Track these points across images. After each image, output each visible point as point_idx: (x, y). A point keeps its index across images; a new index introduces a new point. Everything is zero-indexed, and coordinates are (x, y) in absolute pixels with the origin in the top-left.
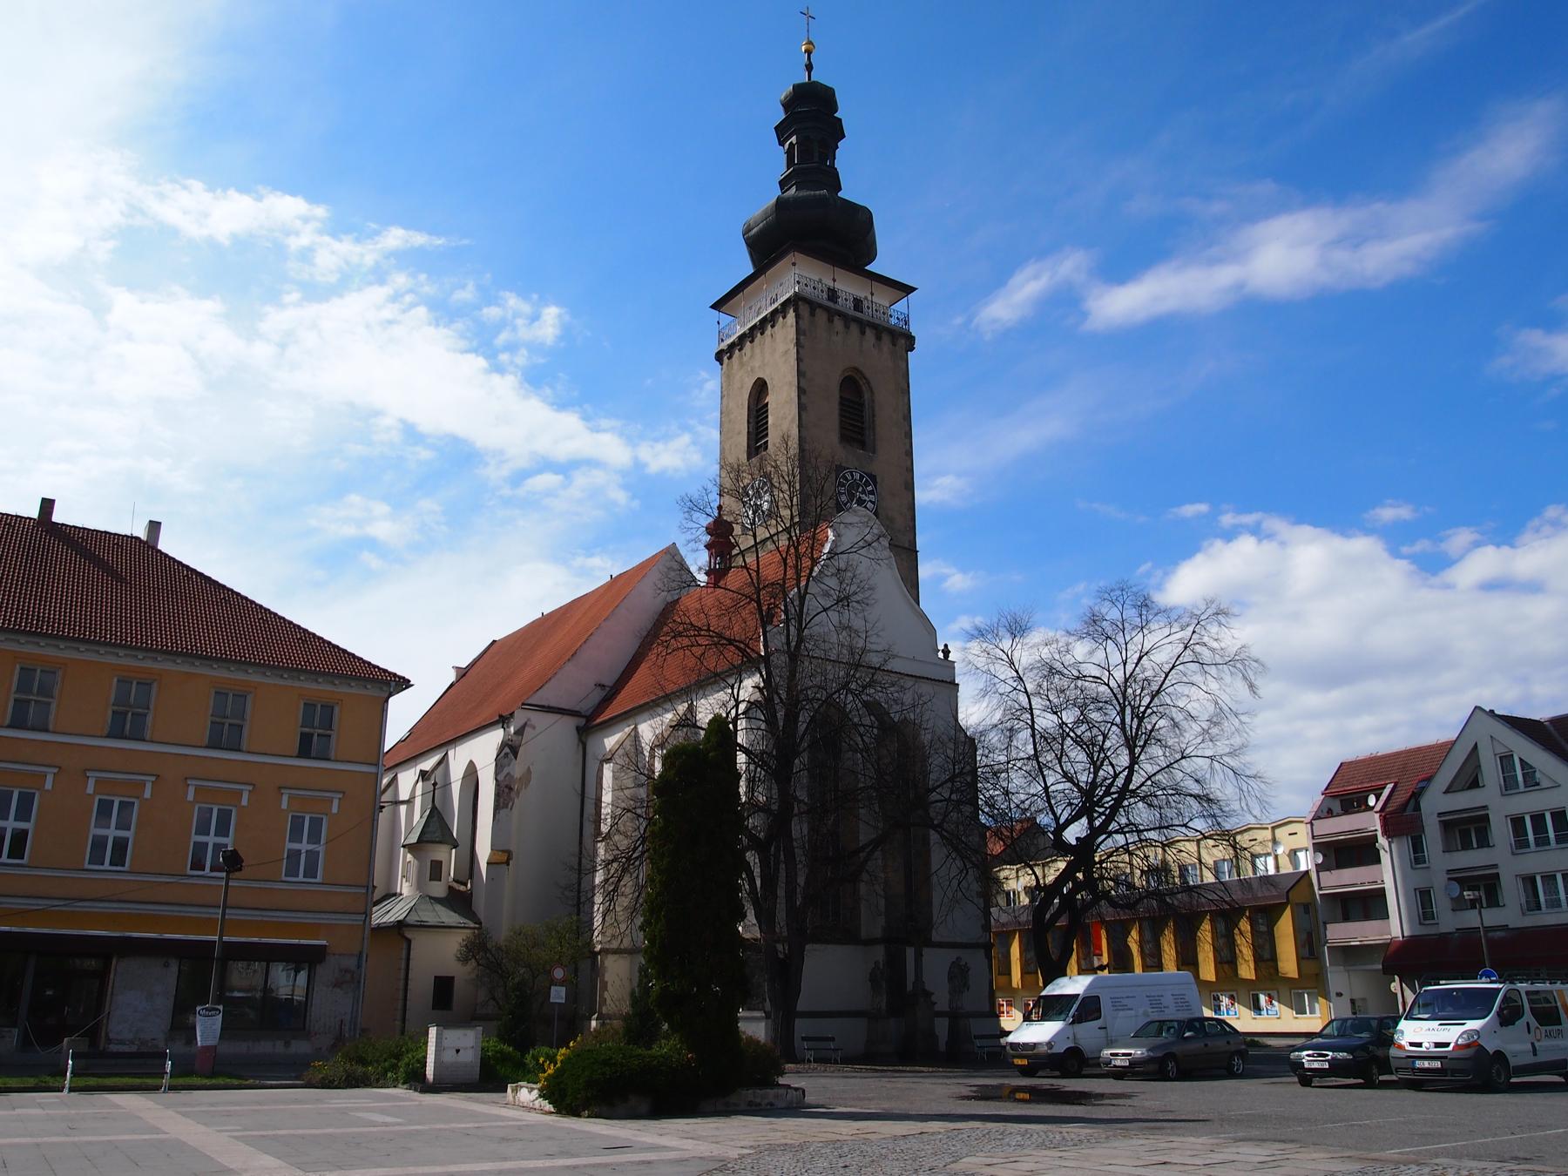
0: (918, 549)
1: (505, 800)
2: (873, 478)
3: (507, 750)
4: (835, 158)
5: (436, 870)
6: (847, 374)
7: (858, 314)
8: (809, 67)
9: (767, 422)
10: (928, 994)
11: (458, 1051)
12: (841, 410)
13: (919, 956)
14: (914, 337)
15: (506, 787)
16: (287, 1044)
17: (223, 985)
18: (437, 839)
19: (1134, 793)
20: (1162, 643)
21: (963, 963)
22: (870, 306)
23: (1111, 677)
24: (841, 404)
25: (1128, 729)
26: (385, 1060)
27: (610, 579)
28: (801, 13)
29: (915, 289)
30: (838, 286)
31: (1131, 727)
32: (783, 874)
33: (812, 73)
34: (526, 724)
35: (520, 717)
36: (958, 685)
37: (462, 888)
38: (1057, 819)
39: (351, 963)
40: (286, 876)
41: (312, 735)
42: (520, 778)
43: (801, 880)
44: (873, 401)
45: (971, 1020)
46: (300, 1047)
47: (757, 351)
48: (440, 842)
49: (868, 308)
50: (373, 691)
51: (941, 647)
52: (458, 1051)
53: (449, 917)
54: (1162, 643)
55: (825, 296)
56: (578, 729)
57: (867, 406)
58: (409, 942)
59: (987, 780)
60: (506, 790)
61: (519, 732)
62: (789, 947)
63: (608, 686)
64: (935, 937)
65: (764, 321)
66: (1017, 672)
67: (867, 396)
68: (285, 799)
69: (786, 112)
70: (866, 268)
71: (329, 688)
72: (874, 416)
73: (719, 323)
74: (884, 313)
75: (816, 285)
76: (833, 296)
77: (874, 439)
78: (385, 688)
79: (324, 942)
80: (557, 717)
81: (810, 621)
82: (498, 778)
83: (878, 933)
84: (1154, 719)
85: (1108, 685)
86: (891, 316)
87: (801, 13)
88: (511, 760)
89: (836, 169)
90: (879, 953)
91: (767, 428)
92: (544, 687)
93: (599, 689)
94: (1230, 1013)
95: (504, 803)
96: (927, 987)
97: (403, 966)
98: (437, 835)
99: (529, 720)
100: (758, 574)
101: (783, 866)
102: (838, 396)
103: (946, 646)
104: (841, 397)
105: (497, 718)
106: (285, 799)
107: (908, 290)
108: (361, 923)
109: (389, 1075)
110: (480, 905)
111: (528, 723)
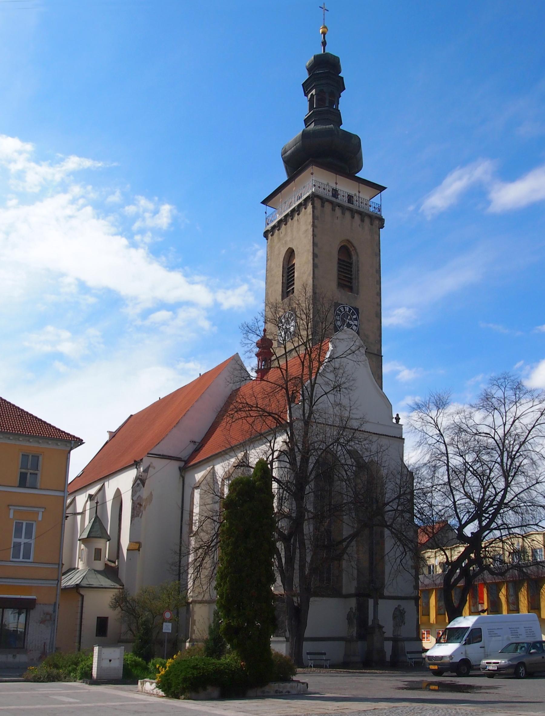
0: (382, 355)
1: (137, 512)
2: (357, 310)
3: (139, 482)
4: (338, 104)
5: (98, 554)
6: (342, 244)
7: (350, 205)
8: (324, 44)
10: (381, 627)
11: (110, 661)
12: (339, 267)
13: (376, 604)
14: (384, 219)
16: (14, 656)
18: (98, 536)
21: (401, 608)
23: (496, 433)
24: (339, 263)
25: (505, 465)
26: (70, 666)
29: (386, 188)
30: (338, 187)
33: (326, 47)
35: (147, 461)
37: (113, 565)
38: (460, 521)
39: (50, 609)
40: (13, 558)
41: (27, 473)
42: (146, 499)
44: (358, 261)
45: (405, 642)
46: (22, 658)
48: (100, 538)
50: (61, 447)
51: (394, 416)
52: (110, 661)
53: (105, 582)
55: (331, 194)
56: (180, 468)
57: (354, 265)
58: (83, 596)
60: (138, 506)
61: (146, 471)
64: (386, 593)
65: (293, 211)
66: (439, 430)
67: (354, 258)
68: (12, 512)
71: (36, 445)
72: (358, 271)
73: (266, 213)
74: (366, 204)
78: (68, 445)
79: (34, 597)
86: (370, 206)
88: (141, 488)
89: (339, 111)
90: (353, 602)
92: (161, 444)
93: (192, 444)
95: (137, 514)
96: (380, 623)
97: (79, 611)
98: (98, 533)
99: (151, 463)
102: (337, 258)
103: (398, 415)
104: (339, 259)
105: (133, 462)
106: (12, 512)
107: (381, 189)
108: (56, 586)
109: (72, 674)
110: (123, 575)
111: (151, 465)
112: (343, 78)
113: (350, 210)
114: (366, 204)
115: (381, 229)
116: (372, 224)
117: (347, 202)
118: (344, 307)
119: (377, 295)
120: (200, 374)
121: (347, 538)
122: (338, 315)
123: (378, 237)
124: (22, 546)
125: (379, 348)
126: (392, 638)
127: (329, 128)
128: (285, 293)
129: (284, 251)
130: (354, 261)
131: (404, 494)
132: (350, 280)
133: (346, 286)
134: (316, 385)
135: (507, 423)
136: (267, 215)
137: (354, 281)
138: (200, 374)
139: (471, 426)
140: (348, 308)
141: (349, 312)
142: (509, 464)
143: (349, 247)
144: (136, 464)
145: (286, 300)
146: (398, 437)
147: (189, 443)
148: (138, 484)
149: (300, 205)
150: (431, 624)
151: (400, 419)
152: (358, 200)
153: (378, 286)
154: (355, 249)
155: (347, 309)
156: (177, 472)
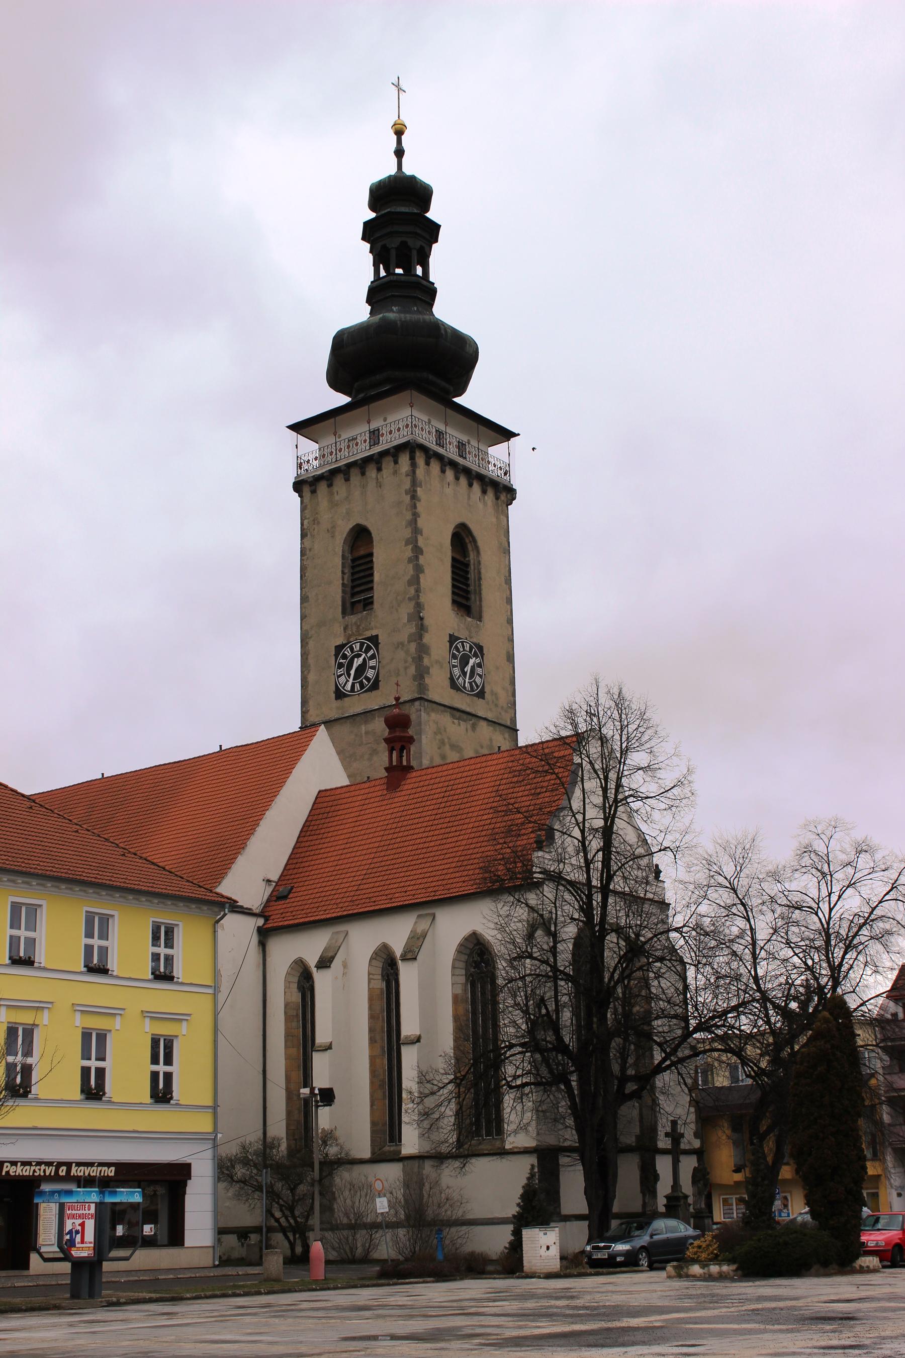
2: (480, 648)
7: (440, 450)
8: (399, 153)
12: (453, 586)
14: (515, 490)
17: (891, 1184)
20: (864, 878)
24: (453, 566)
28: (404, 91)
33: (404, 159)
44: (479, 563)
47: (357, 493)
57: (472, 567)
63: (274, 882)
67: (472, 556)
72: (480, 579)
87: (404, 91)
94: (783, 1214)
104: (453, 559)
107: (506, 435)
116: (497, 498)
117: (434, 443)
118: (462, 643)
119: (508, 623)
120: (221, 746)
122: (340, 666)
124: (20, 1032)
128: (348, 605)
129: (344, 528)
130: (472, 562)
137: (473, 597)
140: (468, 645)
141: (470, 651)
143: (464, 536)
145: (353, 619)
150: (558, 1160)
153: (509, 607)
154: (474, 540)
155: (467, 648)
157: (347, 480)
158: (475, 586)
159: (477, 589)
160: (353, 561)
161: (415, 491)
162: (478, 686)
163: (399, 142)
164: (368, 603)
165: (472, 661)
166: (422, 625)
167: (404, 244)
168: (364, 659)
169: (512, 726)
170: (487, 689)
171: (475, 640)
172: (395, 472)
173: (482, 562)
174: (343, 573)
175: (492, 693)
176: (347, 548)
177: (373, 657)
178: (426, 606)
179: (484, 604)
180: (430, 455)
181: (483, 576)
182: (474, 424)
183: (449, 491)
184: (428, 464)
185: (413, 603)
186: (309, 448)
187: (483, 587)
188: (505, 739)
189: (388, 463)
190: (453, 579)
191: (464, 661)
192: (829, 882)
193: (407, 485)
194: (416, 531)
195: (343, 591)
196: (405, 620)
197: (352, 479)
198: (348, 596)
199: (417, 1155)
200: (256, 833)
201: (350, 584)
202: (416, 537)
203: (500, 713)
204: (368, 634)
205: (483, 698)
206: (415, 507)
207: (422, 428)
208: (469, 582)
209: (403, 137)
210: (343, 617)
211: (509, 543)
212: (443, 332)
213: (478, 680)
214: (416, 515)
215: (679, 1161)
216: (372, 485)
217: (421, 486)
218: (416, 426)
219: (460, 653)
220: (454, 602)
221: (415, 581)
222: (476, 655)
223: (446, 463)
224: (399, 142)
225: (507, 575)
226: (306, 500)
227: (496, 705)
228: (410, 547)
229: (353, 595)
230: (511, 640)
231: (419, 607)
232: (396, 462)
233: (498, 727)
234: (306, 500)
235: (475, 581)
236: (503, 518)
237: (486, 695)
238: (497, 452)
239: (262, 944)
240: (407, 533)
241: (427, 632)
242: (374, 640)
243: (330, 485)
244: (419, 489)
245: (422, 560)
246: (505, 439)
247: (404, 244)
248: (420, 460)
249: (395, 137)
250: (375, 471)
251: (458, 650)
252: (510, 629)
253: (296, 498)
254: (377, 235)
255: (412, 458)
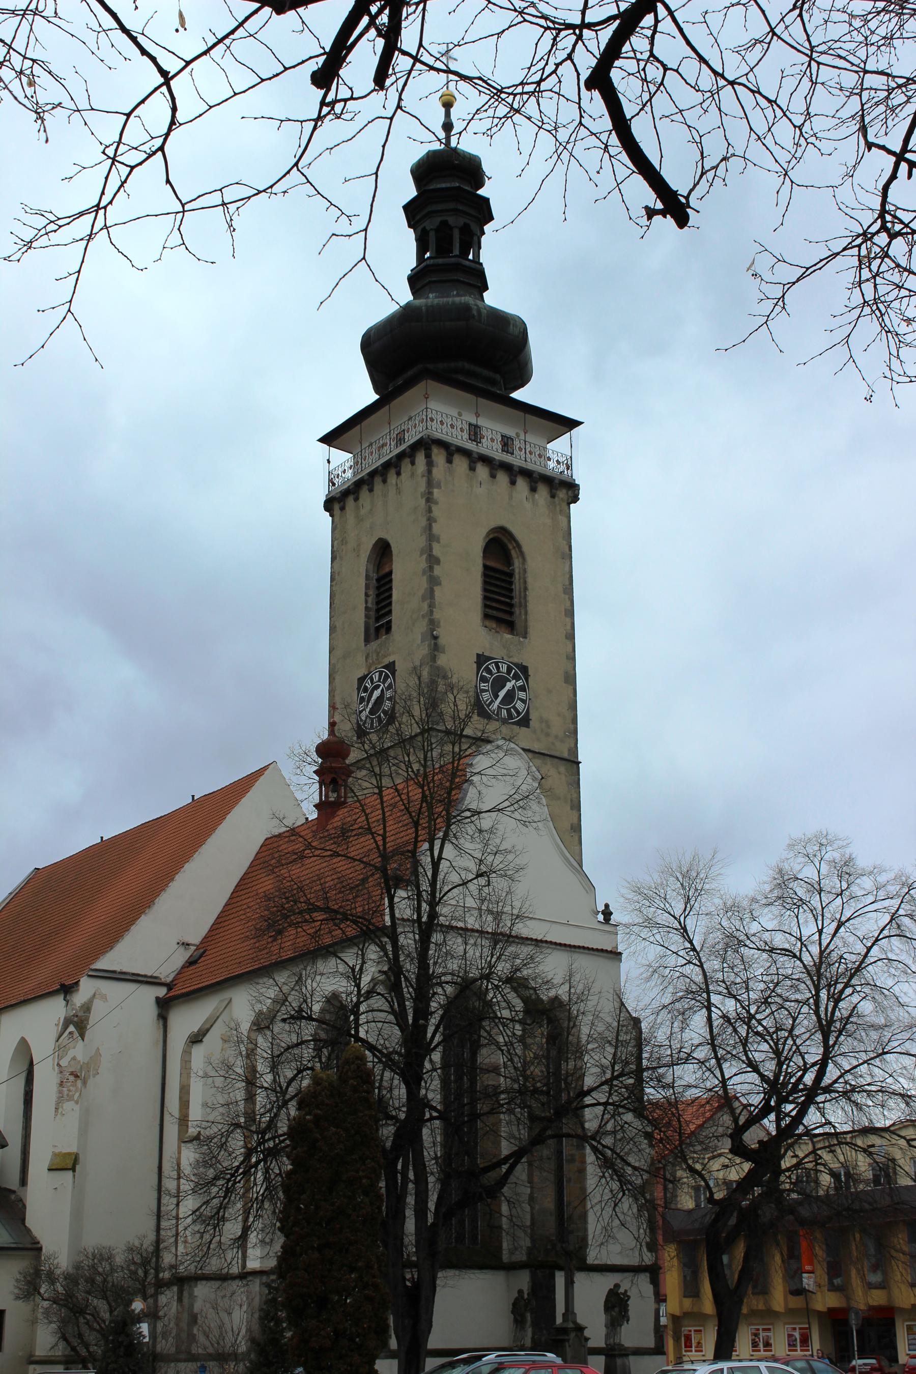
0: (580, 759)
2: (524, 669)
3: (71, 1028)
4: (480, 248)
6: (491, 536)
9: (390, 596)
10: (580, 1329)
12: (485, 598)
13: (570, 1283)
14: (578, 486)
15: (72, 1074)
19: (828, 1090)
20: (866, 909)
21: (622, 1290)
22: (523, 447)
23: (804, 949)
24: (485, 575)
25: (822, 1009)
27: (191, 800)
28: (456, 60)
29: (582, 423)
30: (481, 422)
31: (826, 1009)
32: (411, 1200)
34: (94, 995)
36: (620, 954)
38: (736, 1120)
43: (432, 1206)
44: (525, 571)
45: (631, 1358)
49: (520, 449)
51: (601, 908)
54: (866, 909)
55: (466, 436)
57: (517, 576)
59: (647, 1083)
60: (72, 1078)
62: (418, 1275)
63: (193, 945)
64: (593, 1256)
65: (387, 466)
66: (691, 942)
67: (517, 563)
69: (418, 190)
70: (513, 395)
72: (526, 589)
73: (329, 461)
74: (540, 456)
75: (455, 422)
76: (476, 434)
77: (526, 620)
80: (131, 987)
81: (446, 893)
82: (62, 1063)
83: (521, 1256)
84: (855, 999)
85: (800, 959)
86: (549, 459)
87: (456, 60)
89: (481, 264)
90: (523, 1280)
91: (390, 604)
93: (182, 949)
96: (580, 1320)
100: (384, 839)
101: (411, 1186)
102: (481, 566)
103: (607, 906)
104: (486, 567)
107: (570, 424)
112: (488, 199)
113: (507, 467)
114: (540, 456)
115: (572, 506)
116: (553, 496)
119: (567, 638)
120: (193, 796)
121: (507, 1158)
122: (484, 680)
123: (565, 520)
125: (573, 745)
126: (603, 1348)
127: (461, 303)
128: (372, 631)
129: (368, 544)
130: (517, 571)
131: (622, 1074)
132: (509, 608)
133: (499, 621)
134: (443, 861)
135: (824, 930)
136: (332, 466)
137: (517, 610)
138: (193, 796)
139: (754, 935)
140: (505, 667)
142: (830, 1009)
143: (506, 541)
144: (67, 990)
145: (374, 645)
146: (609, 949)
147: (177, 946)
148: (71, 1033)
149: (401, 456)
151: (611, 913)
152: (523, 447)
153: (568, 620)
154: (518, 546)
155: (504, 669)
156: (151, 1011)
157: (371, 490)
158: (520, 597)
159: (523, 601)
160: (378, 580)
161: (430, 493)
162: (518, 713)
163: (448, 114)
164: (388, 628)
165: (509, 686)
166: (436, 644)
167: (444, 223)
168: (382, 690)
169: (572, 759)
170: (533, 716)
171: (515, 660)
172: (413, 475)
173: (529, 570)
174: (367, 595)
175: (541, 720)
176: (371, 567)
177: (522, 689)
178: (442, 624)
179: (530, 618)
180: (451, 451)
181: (530, 587)
182: (521, 414)
183: (480, 491)
184: (449, 461)
185: (426, 620)
186: (341, 458)
187: (529, 598)
188: (559, 773)
189: (406, 465)
190: (485, 590)
191: (499, 683)
192: (820, 918)
193: (423, 488)
194: (432, 538)
195: (367, 616)
196: (419, 641)
197: (375, 488)
198: (372, 621)
199: (258, 1270)
200: (168, 889)
201: (375, 607)
202: (430, 545)
203: (553, 744)
204: (386, 661)
205: (528, 726)
206: (430, 510)
207: (441, 422)
208: (514, 594)
209: (452, 110)
210: (366, 645)
211: (570, 547)
212: (475, 312)
213: (520, 706)
214: (431, 520)
215: (572, 1282)
216: (392, 491)
217: (439, 487)
218: (432, 420)
219: (492, 675)
220: (486, 616)
221: (430, 595)
222: (516, 677)
223: (475, 459)
224: (448, 114)
225: (567, 583)
226: (337, 519)
227: (548, 735)
228: (425, 556)
229: (378, 619)
230: (572, 658)
231: (433, 624)
232: (413, 463)
233: (548, 759)
234: (337, 519)
235: (520, 592)
236: (562, 519)
237: (531, 723)
238: (559, 447)
239: (163, 1018)
240: (422, 541)
241: (444, 652)
242: (391, 667)
243: (356, 499)
244: (435, 491)
245: (437, 571)
246: (567, 429)
247: (444, 223)
248: (439, 457)
249: (443, 110)
250: (395, 476)
251: (489, 671)
252: (571, 646)
253: (327, 518)
254: (418, 218)
255: (428, 456)
